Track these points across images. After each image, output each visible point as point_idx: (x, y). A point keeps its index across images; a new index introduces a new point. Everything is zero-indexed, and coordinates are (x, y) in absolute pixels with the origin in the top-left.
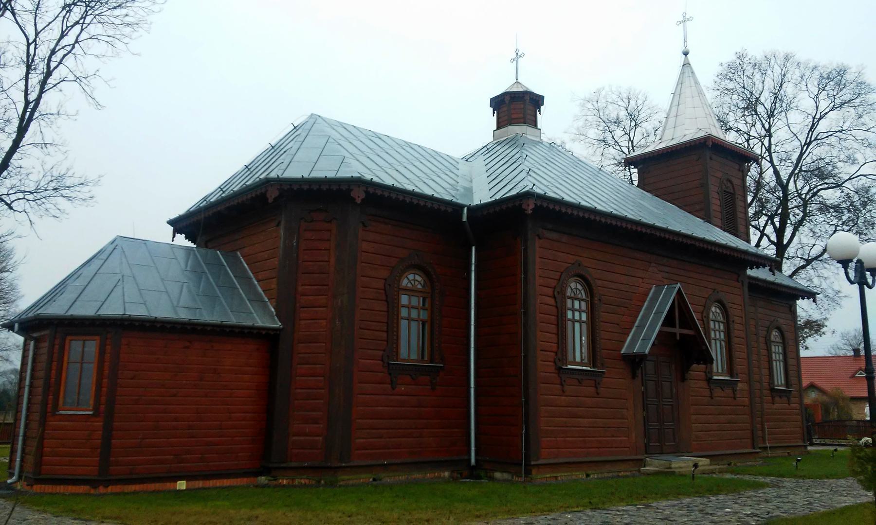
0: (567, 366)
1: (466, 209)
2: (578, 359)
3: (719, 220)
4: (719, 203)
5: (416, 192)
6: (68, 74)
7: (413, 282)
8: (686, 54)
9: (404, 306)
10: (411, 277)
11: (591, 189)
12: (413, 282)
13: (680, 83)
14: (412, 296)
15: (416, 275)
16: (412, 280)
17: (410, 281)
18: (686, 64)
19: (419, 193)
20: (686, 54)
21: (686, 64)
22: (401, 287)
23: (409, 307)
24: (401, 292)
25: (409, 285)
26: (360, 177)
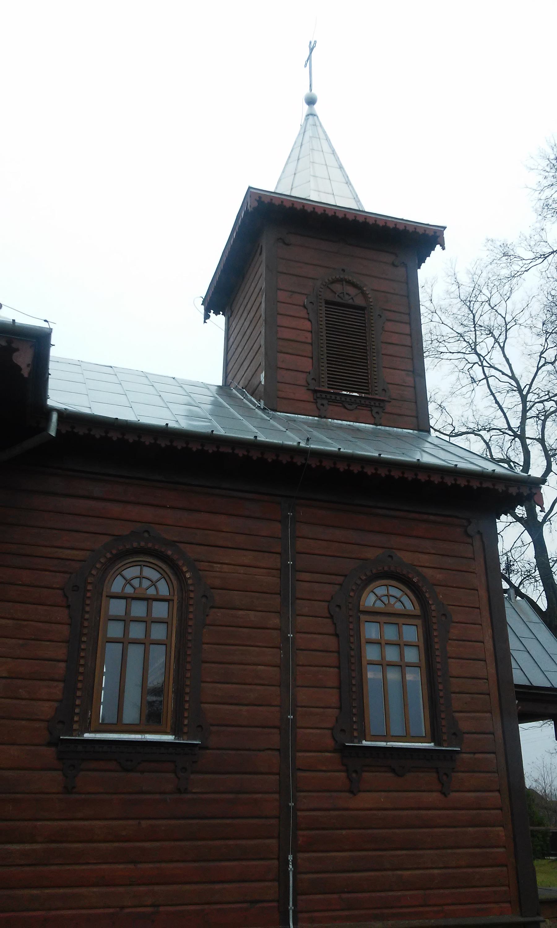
0: (360, 742)
1: (55, 416)
2: (397, 729)
3: (301, 307)
4: (307, 325)
5: (459, 468)
6: (91, 410)
7: (385, 599)
8: (311, 101)
9: (370, 642)
10: (381, 591)
11: (236, 349)
12: (385, 599)
13: (300, 144)
14: (144, 566)
15: (390, 588)
16: (125, 586)
17: (379, 598)
18: (311, 115)
19: (445, 466)
20: (311, 101)
21: (311, 115)
22: (361, 608)
23: (380, 643)
24: (363, 617)
25: (379, 604)
26: (483, 471)
